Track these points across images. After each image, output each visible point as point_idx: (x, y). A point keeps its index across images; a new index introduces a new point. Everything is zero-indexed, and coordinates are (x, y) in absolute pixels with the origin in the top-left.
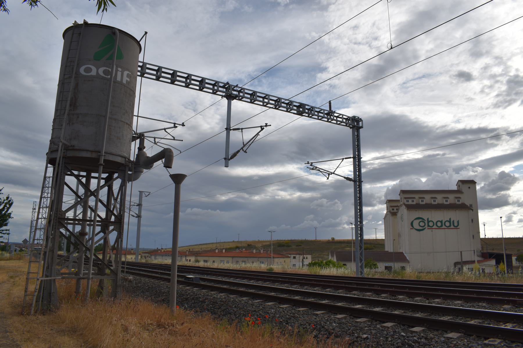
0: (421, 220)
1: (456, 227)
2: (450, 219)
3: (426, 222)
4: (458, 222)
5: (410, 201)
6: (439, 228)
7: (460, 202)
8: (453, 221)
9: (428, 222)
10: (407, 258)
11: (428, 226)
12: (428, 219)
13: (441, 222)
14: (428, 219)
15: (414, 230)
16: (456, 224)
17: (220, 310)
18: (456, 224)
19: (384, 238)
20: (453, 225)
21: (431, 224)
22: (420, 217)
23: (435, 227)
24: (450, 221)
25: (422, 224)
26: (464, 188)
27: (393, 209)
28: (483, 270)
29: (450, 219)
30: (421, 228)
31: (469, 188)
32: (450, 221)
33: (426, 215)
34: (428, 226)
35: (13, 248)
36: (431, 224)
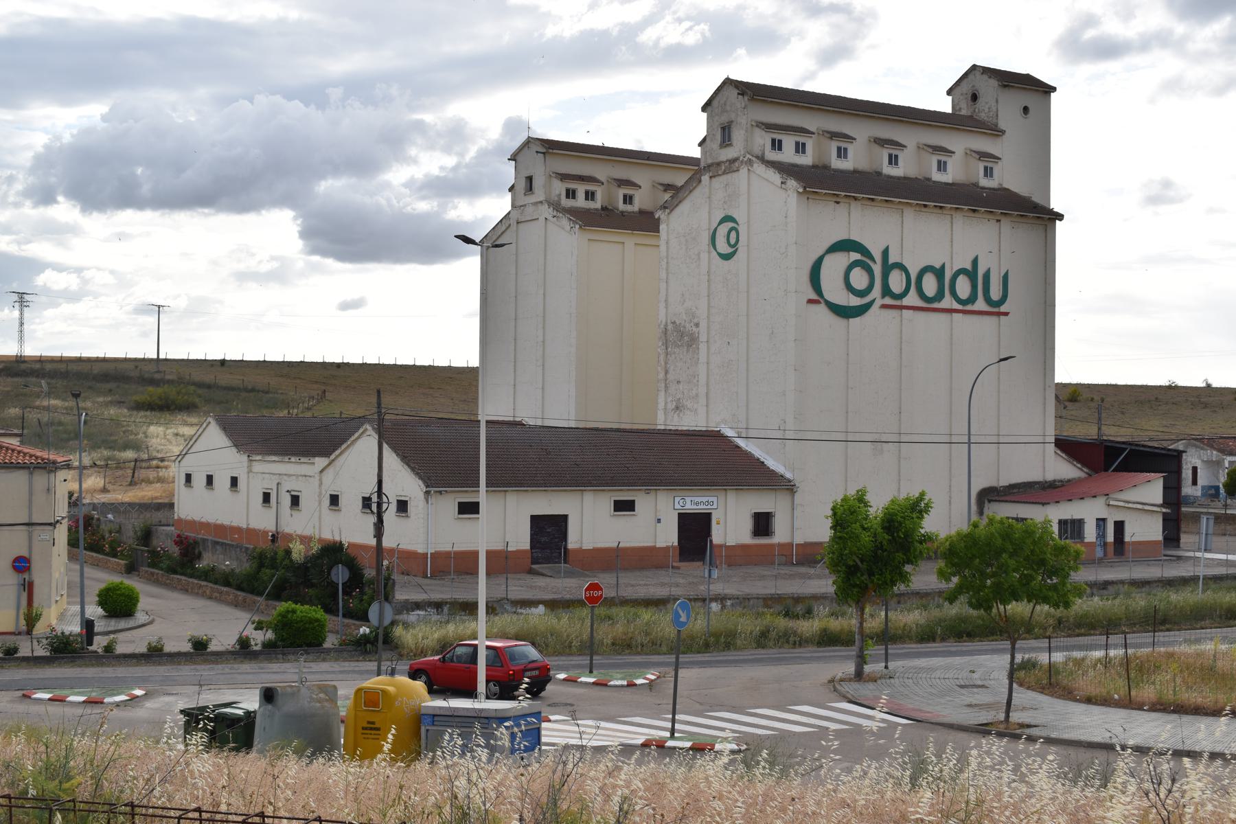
0: (855, 256)
1: (996, 308)
2: (975, 262)
3: (877, 269)
4: (1005, 278)
5: (789, 142)
6: (929, 305)
7: (963, 175)
8: (987, 276)
9: (887, 268)
10: (771, 463)
11: (886, 291)
12: (885, 253)
13: (939, 273)
14: (885, 253)
15: (822, 309)
16: (995, 294)
17: (867, 782)
18: (995, 294)
19: (475, 362)
20: (942, 291)
21: (896, 282)
22: (855, 237)
23: (912, 299)
24: (971, 274)
25: (859, 279)
26: (1006, 109)
27: (571, 194)
28: (1119, 526)
29: (975, 262)
30: (855, 301)
31: (1026, 110)
32: (971, 274)
33: (876, 227)
34: (886, 291)
35: (335, 93)
36: (896, 282)
